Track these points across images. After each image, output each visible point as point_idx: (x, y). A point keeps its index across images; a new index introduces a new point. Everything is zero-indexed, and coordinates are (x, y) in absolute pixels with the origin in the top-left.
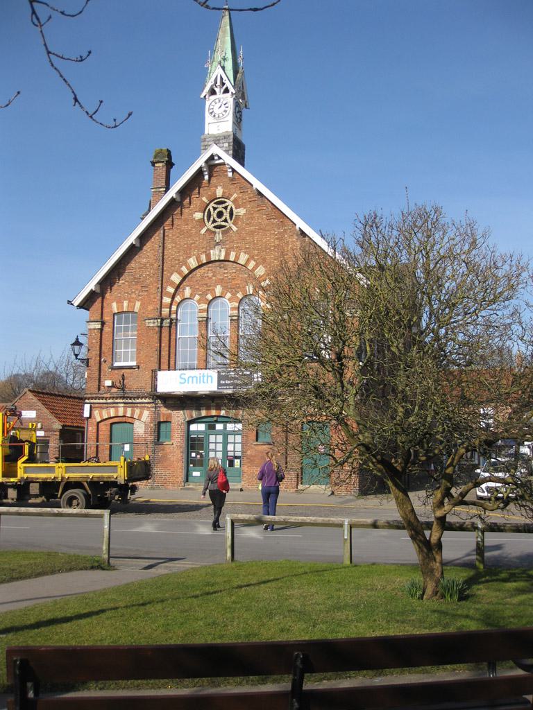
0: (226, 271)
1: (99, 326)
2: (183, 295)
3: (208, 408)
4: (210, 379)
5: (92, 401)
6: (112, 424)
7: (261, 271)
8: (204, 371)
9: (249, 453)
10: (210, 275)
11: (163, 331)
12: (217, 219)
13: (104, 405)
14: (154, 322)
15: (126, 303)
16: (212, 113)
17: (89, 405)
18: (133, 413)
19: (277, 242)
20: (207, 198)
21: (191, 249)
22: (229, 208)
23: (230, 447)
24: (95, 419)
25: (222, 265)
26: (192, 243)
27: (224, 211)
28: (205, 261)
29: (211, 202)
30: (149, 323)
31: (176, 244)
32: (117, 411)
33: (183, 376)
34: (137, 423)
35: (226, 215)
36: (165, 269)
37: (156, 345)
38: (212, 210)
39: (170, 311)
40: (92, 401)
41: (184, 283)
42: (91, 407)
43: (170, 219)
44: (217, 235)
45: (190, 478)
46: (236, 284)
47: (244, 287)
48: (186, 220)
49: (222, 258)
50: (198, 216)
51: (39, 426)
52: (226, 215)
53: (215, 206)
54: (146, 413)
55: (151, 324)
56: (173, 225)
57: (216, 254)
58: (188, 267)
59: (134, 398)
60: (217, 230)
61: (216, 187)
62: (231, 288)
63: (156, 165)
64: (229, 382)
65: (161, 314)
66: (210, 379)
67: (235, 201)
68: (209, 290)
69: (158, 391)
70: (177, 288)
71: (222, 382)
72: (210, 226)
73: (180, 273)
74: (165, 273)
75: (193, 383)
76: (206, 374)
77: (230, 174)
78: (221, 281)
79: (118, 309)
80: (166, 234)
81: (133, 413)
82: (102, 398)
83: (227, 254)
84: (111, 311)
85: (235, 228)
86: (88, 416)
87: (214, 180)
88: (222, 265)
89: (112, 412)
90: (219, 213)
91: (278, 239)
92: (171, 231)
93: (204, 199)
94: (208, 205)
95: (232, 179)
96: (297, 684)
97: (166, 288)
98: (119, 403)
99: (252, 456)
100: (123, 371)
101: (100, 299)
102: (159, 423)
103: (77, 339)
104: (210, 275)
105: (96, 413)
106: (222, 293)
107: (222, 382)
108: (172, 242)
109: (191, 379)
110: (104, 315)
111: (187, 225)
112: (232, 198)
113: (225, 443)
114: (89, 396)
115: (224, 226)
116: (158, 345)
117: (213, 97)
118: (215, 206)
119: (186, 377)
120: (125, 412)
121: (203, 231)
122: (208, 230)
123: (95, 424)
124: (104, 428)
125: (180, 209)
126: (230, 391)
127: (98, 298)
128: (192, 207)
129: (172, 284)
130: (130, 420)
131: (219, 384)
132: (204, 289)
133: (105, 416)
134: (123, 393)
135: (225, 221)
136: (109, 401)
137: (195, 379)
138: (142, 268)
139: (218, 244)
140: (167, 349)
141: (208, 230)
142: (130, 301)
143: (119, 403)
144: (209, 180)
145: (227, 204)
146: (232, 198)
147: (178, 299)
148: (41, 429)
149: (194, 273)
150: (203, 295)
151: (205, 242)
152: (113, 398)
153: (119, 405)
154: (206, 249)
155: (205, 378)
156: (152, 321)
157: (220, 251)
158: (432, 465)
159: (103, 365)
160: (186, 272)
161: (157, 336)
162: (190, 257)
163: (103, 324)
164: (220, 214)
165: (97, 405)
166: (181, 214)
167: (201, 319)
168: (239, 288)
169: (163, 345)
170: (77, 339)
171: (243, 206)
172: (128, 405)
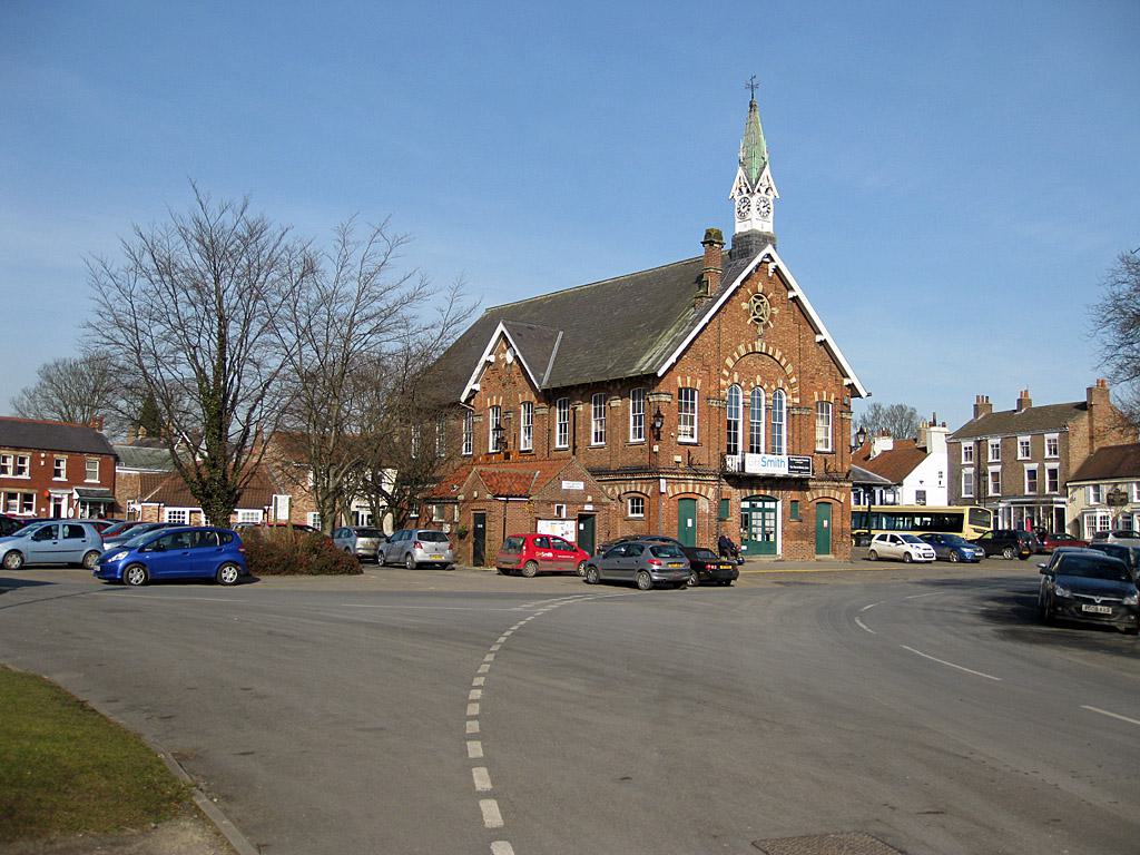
3: (758, 489)
7: (789, 369)
23: (767, 523)
34: (701, 499)
48: (735, 307)
54: (711, 490)
57: (760, 346)
59: (704, 475)
78: (760, 372)
96: (487, 795)
113: (764, 520)
121: (749, 322)
126: (797, 476)
130: (695, 496)
134: (694, 470)
139: (760, 337)
158: (565, 485)
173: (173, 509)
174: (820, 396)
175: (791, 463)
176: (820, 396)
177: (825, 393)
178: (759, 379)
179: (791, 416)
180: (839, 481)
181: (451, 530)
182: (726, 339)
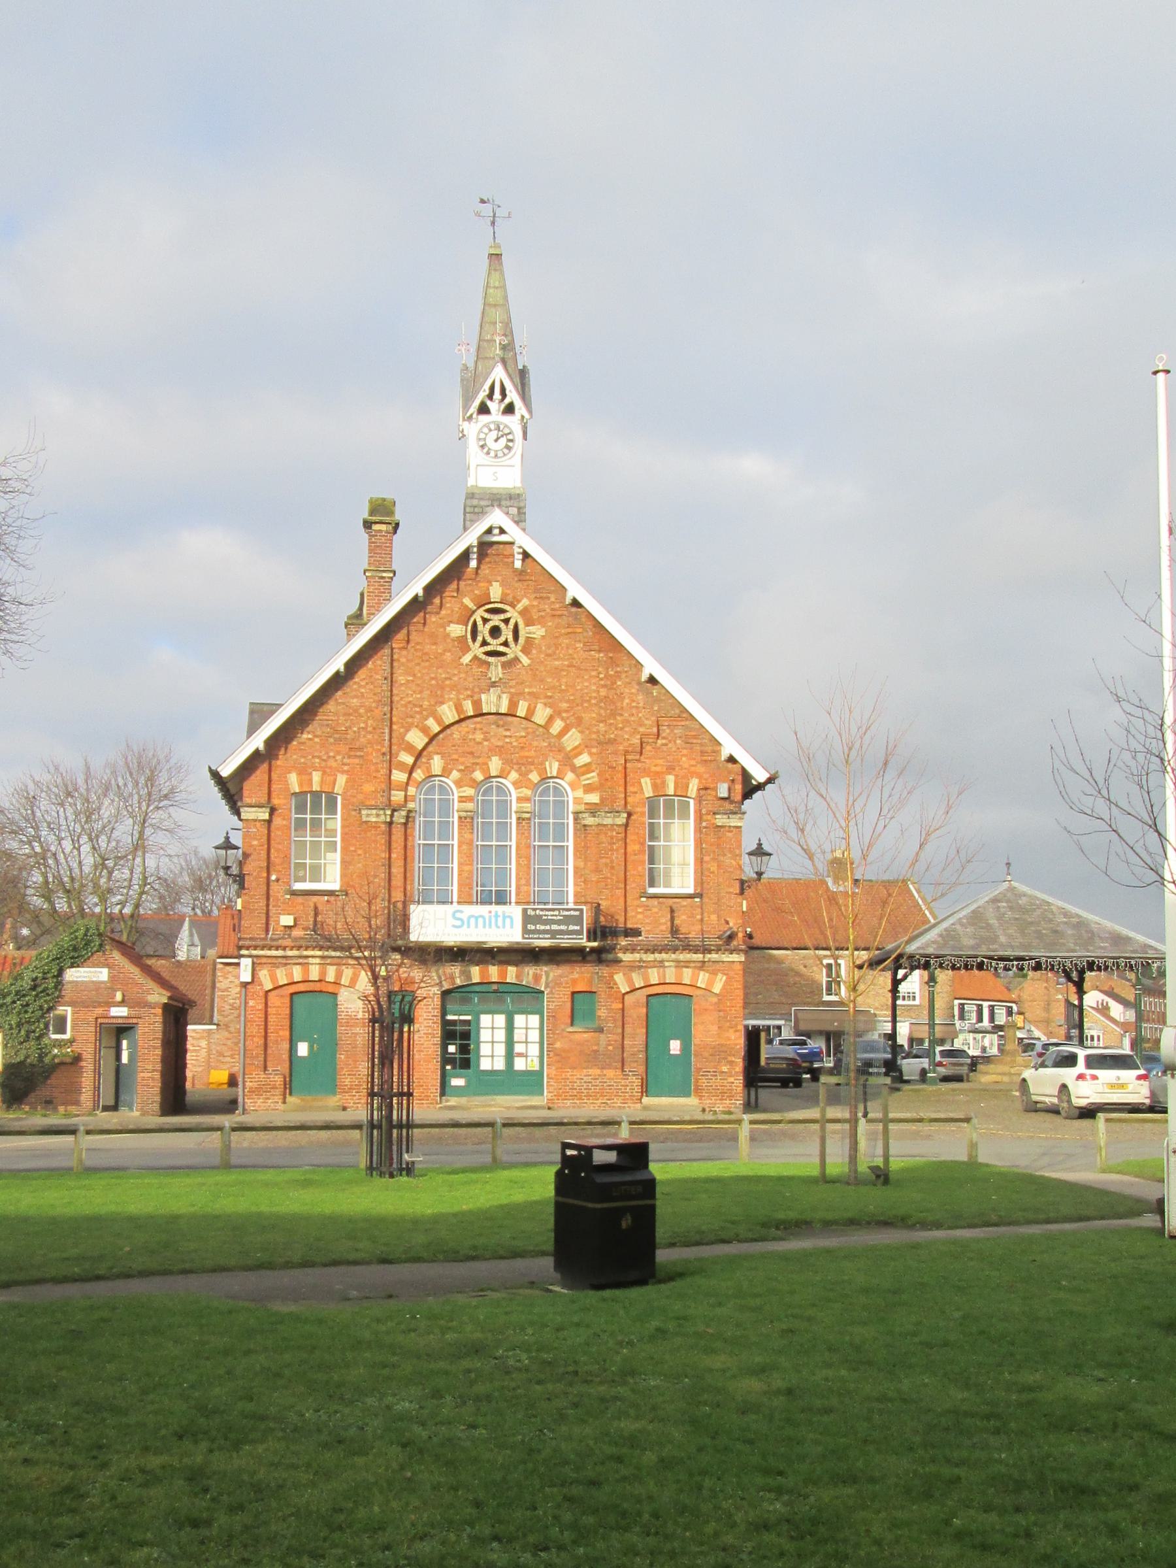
0: (508, 733)
1: (267, 816)
2: (429, 769)
4: (508, 921)
5: (254, 952)
6: (292, 994)
7: (573, 739)
8: (494, 908)
9: (558, 1045)
10: (479, 737)
11: (394, 831)
12: (489, 639)
13: (280, 960)
14: (378, 815)
15: (316, 777)
16: (482, 447)
17: (250, 960)
18: (339, 975)
19: (603, 692)
20: (472, 600)
21: (442, 688)
22: (512, 622)
24: (261, 984)
25: (501, 723)
26: (446, 679)
27: (502, 626)
28: (471, 713)
29: (479, 608)
30: (368, 815)
31: (414, 675)
32: (306, 971)
33: (458, 915)
35: (507, 633)
36: (394, 719)
37: (383, 855)
38: (480, 622)
39: (406, 796)
40: (254, 952)
41: (430, 748)
42: (253, 963)
43: (404, 631)
44: (492, 668)
45: (447, 1089)
46: (527, 757)
47: (542, 763)
48: (433, 636)
49: (503, 710)
50: (456, 630)
51: (119, 996)
52: (507, 633)
53: (487, 616)
55: (371, 816)
56: (408, 642)
57: (493, 701)
58: (439, 720)
60: (491, 659)
61: (490, 582)
62: (518, 763)
63: (376, 527)
64: (543, 927)
65: (390, 801)
66: (508, 921)
67: (524, 613)
68: (477, 764)
69: (413, 937)
70: (419, 756)
71: (531, 927)
72: (477, 650)
73: (425, 730)
74: (394, 727)
75: (476, 926)
76: (500, 913)
77: (518, 564)
78: (499, 751)
79: (301, 785)
80: (395, 657)
81: (339, 975)
82: (277, 948)
83: (513, 704)
84: (287, 789)
85: (525, 660)
86: (249, 980)
87: (485, 570)
88: (501, 723)
89: (297, 973)
90: (495, 634)
91: (604, 686)
92: (404, 652)
93: (467, 601)
94: (474, 612)
95: (521, 573)
97: (397, 755)
98: (313, 957)
99: (564, 1051)
100: (315, 899)
101: (265, 766)
102: (573, 993)
103: (227, 838)
104: (479, 737)
105: (264, 974)
106: (502, 770)
107: (531, 927)
108: (407, 673)
109: (473, 921)
110: (274, 795)
111: (435, 644)
112: (520, 607)
114: (247, 943)
115: (474, 639)
116: (385, 855)
117: (484, 419)
118: (487, 616)
119: (464, 916)
120: (323, 973)
121: (467, 659)
122: (476, 658)
123: (262, 994)
124: (279, 1003)
125: (422, 614)
127: (263, 762)
128: (443, 612)
129: (409, 748)
130: (331, 989)
131: (525, 931)
132: (468, 761)
133: (283, 981)
135: (506, 644)
136: (290, 953)
137: (480, 921)
138: (350, 715)
139: (493, 685)
140: (401, 863)
141: (476, 658)
142: (324, 773)
143: (313, 957)
144: (478, 568)
145: (508, 615)
146: (520, 607)
147: (418, 775)
148: (123, 1003)
149: (448, 731)
150: (467, 770)
151: (471, 679)
152: (299, 948)
153: (311, 960)
154: (473, 691)
155: (500, 920)
156: (374, 812)
157: (499, 697)
159: (274, 887)
160: (436, 728)
161: (382, 840)
162: (442, 703)
163: (273, 811)
164: (495, 632)
165: (264, 960)
166: (424, 624)
167: (464, 814)
168: (532, 763)
169: (394, 856)
170: (227, 838)
171: (541, 621)
172: (329, 961)
173: (911, 1003)
174: (658, 787)
175: (527, 919)
176: (658, 787)
177: (670, 780)
178: (495, 764)
179: (582, 829)
180: (706, 950)
181: (159, 1556)
182: (406, 693)
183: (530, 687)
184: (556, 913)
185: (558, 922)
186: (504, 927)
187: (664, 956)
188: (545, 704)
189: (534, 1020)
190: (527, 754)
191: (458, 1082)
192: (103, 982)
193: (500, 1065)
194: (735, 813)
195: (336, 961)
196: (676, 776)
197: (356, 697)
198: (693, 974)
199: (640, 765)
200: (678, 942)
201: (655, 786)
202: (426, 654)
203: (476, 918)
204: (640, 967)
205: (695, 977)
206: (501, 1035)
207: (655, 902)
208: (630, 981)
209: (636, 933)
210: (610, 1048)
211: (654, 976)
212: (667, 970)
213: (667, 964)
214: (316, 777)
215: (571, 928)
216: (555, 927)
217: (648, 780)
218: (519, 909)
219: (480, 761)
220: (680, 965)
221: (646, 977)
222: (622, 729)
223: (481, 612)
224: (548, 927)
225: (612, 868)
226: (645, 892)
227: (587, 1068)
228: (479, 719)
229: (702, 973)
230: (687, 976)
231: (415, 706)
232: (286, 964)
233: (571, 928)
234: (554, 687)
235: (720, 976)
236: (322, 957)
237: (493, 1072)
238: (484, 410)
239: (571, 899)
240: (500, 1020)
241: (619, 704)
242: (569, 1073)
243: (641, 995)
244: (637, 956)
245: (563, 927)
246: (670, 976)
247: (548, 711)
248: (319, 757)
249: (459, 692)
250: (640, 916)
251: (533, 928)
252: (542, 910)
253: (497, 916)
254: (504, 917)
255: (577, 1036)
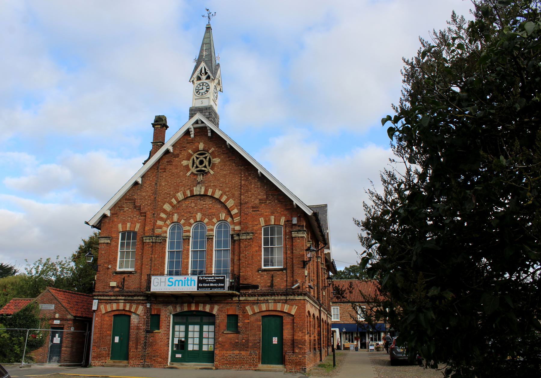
2: (172, 219)
5: (99, 298)
10: (193, 205)
14: (150, 239)
24: (101, 311)
27: (204, 160)
32: (118, 306)
33: (171, 280)
38: (195, 159)
40: (99, 298)
47: (218, 215)
48: (176, 166)
49: (202, 193)
53: (198, 156)
63: (156, 126)
64: (206, 285)
71: (200, 285)
78: (201, 210)
79: (122, 228)
83: (206, 190)
86: (96, 309)
93: (190, 151)
98: (121, 299)
106: (202, 219)
107: (200, 285)
109: (177, 282)
111: (177, 169)
118: (208, 157)
119: (173, 280)
122: (192, 173)
130: (128, 313)
137: (180, 282)
139: (199, 183)
141: (192, 173)
142: (132, 223)
143: (121, 299)
146: (210, 151)
155: (189, 282)
157: (201, 188)
162: (178, 192)
167: (185, 238)
174: (267, 221)
177: (272, 218)
183: (214, 183)
184: (213, 278)
185: (214, 283)
186: (191, 285)
187: (269, 298)
188: (219, 190)
189: (212, 328)
190: (212, 211)
191: (179, 356)
192: (52, 310)
193: (196, 348)
194: (301, 231)
195: (130, 301)
196: (275, 216)
197: (145, 192)
198: (282, 305)
199: (259, 212)
200: (271, 292)
201: (265, 221)
202: (174, 173)
203: (179, 281)
204: (257, 303)
205: (283, 307)
206: (197, 335)
207: (266, 273)
208: (253, 310)
209: (256, 287)
210: (244, 341)
211: (264, 307)
212: (270, 304)
213: (270, 301)
214: (128, 225)
215: (220, 285)
216: (212, 285)
217: (262, 218)
218: (195, 278)
219: (193, 215)
220: (276, 301)
221: (260, 308)
222: (251, 197)
223: (196, 155)
224: (208, 285)
225: (246, 258)
226: (261, 268)
227: (233, 350)
228: (193, 198)
229: (286, 305)
230: (279, 307)
231: (168, 194)
232: (111, 303)
233: (220, 285)
234: (223, 182)
235: (294, 306)
236: (124, 300)
237: (193, 351)
238: (199, 79)
239: (213, 272)
240: (197, 328)
241: (250, 187)
242: (225, 352)
243: (259, 317)
244: (256, 298)
245: (215, 285)
246: (271, 306)
247: (221, 192)
248: (130, 217)
249: (185, 187)
250: (259, 280)
251: (202, 285)
252: (206, 277)
253: (188, 280)
254: (191, 281)
255: (229, 335)
